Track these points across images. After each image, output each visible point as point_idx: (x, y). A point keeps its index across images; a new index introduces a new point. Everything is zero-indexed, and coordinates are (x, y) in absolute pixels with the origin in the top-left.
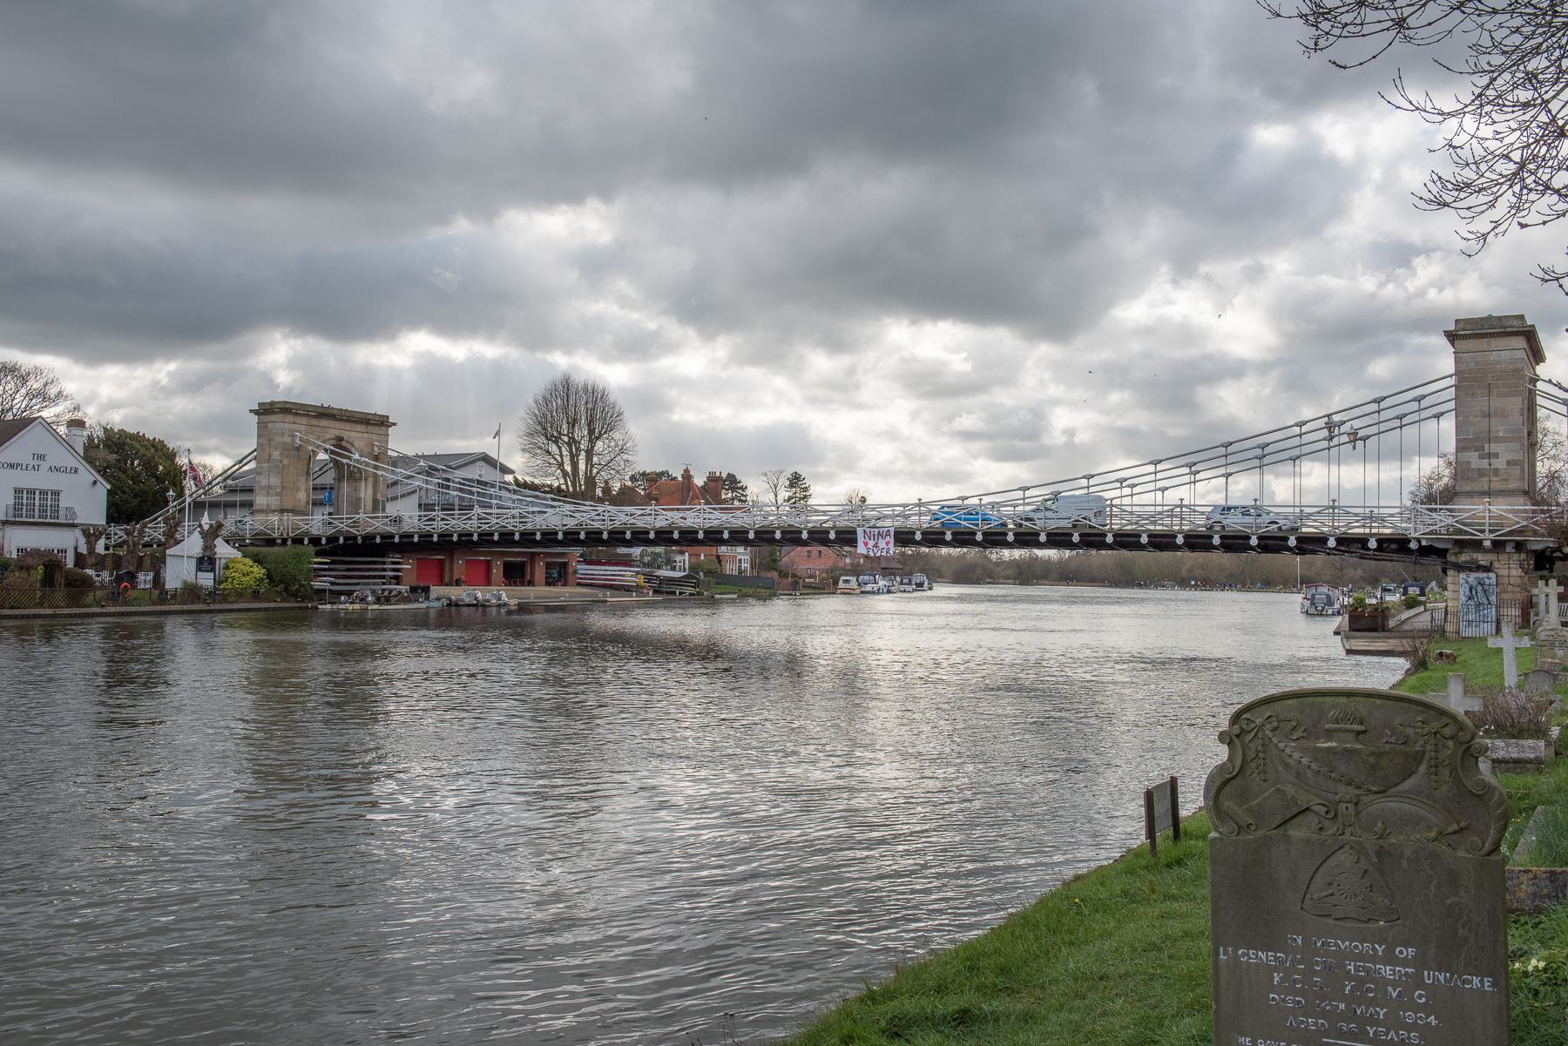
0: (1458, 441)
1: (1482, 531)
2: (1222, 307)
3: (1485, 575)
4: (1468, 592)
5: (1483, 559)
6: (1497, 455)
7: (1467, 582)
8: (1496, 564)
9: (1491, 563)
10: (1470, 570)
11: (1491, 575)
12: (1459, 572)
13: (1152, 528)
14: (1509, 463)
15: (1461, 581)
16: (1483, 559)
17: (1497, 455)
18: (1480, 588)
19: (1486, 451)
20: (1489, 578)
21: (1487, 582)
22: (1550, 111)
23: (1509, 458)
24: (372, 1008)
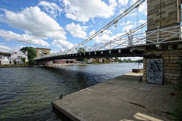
0: (148, 12)
1: (156, 41)
2: (124, 59)
3: (158, 59)
4: (150, 66)
5: (157, 53)
6: (164, 12)
7: (150, 62)
8: (163, 55)
9: (161, 55)
10: (152, 58)
11: (160, 59)
12: (147, 59)
13: (90, 51)
14: (170, 14)
15: (148, 62)
16: (157, 53)
17: (164, 12)
18: (155, 65)
19: (160, 11)
20: (160, 61)
21: (159, 62)
22: (161, 17)
23: (170, 11)
24: (131, 104)
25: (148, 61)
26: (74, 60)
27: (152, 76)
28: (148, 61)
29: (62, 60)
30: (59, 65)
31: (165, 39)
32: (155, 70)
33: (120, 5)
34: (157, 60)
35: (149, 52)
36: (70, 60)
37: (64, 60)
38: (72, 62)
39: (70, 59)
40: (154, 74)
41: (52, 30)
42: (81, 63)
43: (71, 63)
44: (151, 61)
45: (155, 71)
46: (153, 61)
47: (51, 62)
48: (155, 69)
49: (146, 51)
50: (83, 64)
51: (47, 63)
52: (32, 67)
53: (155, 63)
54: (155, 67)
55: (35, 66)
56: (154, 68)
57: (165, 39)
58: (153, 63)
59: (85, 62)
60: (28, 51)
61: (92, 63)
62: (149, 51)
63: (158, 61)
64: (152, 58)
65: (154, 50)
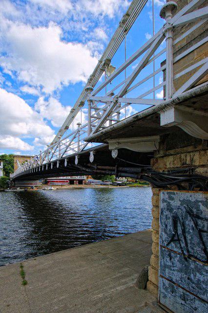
18: (190, 223)
25: (164, 201)
26: (85, 177)
27: (176, 276)
28: (164, 201)
29: (62, 178)
30: (53, 188)
31: (199, 67)
32: (188, 251)
33: (105, 29)
34: (197, 201)
35: (171, 159)
36: (78, 178)
37: (65, 178)
38: (80, 182)
39: (77, 176)
40: (186, 270)
41: (17, 120)
42: (101, 184)
43: (79, 184)
44: (172, 202)
45: (187, 257)
46: (183, 202)
47: (39, 183)
48: (187, 245)
49: (162, 153)
50: (104, 187)
51: (31, 184)
52: (4, 191)
53: (189, 212)
54: (189, 237)
55: (8, 190)
56: (185, 238)
57: (199, 67)
58: (179, 213)
59: (109, 183)
60: (112, 162)
61: (126, 185)
62: (172, 152)
63: (202, 207)
64: (181, 188)
65: (190, 149)
